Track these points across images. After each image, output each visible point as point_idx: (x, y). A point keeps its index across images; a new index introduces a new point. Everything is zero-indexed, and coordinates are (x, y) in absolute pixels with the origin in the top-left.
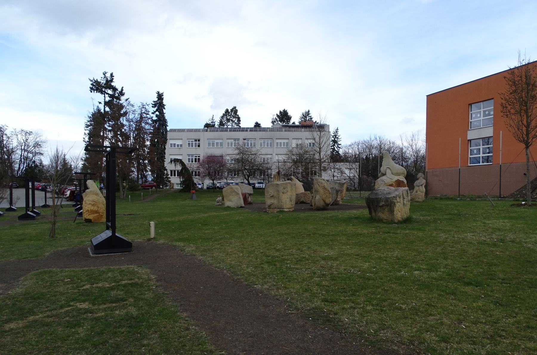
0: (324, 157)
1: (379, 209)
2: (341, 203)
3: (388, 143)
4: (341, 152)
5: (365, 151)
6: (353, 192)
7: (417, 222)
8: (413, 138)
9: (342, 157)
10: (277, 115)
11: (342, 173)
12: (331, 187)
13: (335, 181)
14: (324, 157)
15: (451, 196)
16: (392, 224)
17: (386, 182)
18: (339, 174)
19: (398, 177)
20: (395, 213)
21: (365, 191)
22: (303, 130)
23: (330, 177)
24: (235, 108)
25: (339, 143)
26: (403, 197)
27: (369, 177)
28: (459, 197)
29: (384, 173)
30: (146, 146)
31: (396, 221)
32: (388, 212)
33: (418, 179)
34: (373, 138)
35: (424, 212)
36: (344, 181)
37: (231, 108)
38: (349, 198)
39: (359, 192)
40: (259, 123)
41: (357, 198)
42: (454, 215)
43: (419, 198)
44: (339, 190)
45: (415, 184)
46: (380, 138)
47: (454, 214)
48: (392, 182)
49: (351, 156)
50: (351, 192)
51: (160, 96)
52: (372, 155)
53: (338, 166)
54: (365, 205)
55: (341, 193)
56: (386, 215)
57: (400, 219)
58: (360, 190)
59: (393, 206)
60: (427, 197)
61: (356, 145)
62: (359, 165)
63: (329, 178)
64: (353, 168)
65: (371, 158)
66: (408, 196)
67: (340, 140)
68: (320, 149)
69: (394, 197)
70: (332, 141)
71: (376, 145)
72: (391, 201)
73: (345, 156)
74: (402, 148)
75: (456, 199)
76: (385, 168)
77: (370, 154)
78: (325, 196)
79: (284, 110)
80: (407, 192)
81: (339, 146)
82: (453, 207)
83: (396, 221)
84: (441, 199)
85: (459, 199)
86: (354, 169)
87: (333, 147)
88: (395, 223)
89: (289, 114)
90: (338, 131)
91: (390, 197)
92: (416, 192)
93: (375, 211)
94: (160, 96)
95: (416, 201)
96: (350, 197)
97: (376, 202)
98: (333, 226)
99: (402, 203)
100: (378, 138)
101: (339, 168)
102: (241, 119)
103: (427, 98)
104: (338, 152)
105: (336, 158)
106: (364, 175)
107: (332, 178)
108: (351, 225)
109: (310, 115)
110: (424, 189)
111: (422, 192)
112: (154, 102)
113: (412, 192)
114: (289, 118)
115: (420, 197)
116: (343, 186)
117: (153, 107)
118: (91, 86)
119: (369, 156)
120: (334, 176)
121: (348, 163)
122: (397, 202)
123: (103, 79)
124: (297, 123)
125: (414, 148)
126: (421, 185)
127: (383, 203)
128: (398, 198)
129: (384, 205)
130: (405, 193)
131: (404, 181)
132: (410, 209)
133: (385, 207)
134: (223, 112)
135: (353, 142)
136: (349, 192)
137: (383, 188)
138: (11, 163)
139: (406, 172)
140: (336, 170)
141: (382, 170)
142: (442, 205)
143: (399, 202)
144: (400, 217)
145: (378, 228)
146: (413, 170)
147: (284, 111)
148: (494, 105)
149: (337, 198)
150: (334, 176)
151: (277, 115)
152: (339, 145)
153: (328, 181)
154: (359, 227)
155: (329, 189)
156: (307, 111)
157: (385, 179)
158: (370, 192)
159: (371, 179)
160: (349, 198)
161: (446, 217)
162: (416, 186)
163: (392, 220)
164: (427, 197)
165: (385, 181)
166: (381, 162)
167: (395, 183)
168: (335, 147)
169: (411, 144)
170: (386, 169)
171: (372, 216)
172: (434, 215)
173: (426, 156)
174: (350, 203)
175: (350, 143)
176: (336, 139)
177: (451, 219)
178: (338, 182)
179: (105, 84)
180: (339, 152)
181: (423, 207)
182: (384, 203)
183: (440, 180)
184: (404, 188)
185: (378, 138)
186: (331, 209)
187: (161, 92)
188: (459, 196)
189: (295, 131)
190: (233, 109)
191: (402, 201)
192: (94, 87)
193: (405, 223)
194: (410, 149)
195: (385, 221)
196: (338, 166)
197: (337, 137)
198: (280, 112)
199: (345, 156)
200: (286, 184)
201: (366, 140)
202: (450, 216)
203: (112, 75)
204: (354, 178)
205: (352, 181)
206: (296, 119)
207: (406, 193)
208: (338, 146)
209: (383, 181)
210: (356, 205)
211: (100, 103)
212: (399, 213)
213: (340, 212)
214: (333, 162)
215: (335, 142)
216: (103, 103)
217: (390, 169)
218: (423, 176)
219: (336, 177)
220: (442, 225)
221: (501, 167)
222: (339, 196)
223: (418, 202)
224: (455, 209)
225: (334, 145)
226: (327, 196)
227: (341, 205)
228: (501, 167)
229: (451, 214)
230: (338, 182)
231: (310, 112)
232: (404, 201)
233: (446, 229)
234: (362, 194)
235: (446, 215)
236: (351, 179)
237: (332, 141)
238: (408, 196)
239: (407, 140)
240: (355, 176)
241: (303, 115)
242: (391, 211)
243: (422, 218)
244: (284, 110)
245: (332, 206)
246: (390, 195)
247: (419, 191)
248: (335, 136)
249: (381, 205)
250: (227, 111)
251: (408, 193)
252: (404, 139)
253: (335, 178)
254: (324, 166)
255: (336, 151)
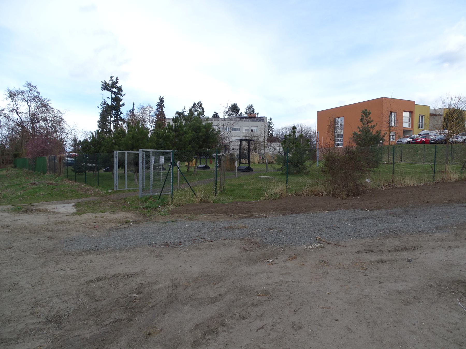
4: (274, 134)
9: (274, 137)
10: (230, 107)
22: (250, 120)
24: (200, 102)
25: (273, 128)
30: (293, 154)
37: (198, 102)
40: (217, 112)
46: (301, 125)
49: (281, 137)
51: (162, 100)
67: (273, 125)
68: (264, 138)
79: (235, 103)
81: (273, 130)
89: (238, 107)
90: (271, 119)
94: (162, 100)
100: (299, 125)
102: (205, 110)
103: (317, 113)
105: (271, 139)
109: (253, 108)
112: (158, 103)
114: (238, 110)
117: (157, 106)
118: (102, 86)
120: (270, 151)
123: (110, 81)
124: (244, 115)
134: (192, 105)
138: (88, 141)
147: (235, 104)
148: (344, 119)
151: (230, 107)
152: (273, 129)
156: (251, 105)
168: (269, 130)
176: (270, 125)
179: (112, 85)
185: (299, 125)
187: (162, 97)
189: (244, 121)
190: (199, 103)
192: (104, 87)
197: (271, 123)
198: (232, 105)
200: (256, 154)
203: (117, 78)
206: (243, 110)
208: (272, 130)
211: (108, 98)
215: (270, 127)
216: (111, 98)
231: (253, 106)
241: (248, 107)
244: (235, 103)
248: (270, 123)
250: (195, 104)
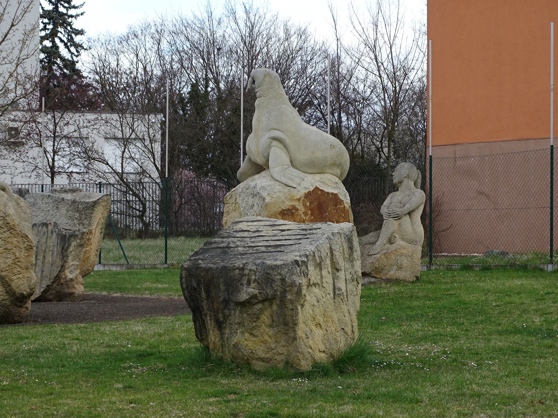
0: (12, 86)
1: (236, 316)
2: (79, 289)
3: (282, 35)
5: (186, 64)
6: (136, 242)
7: (389, 366)
8: (381, 18)
11: (89, 158)
12: (38, 220)
13: (57, 195)
14: (12, 86)
15: (525, 257)
16: (290, 377)
17: (268, 200)
18: (78, 161)
19: (318, 177)
20: (300, 333)
21: (189, 235)
23: (38, 176)
25: (77, 24)
26: (332, 260)
27: (206, 175)
28: (551, 262)
29: (260, 160)
31: (305, 365)
32: (270, 326)
33: (395, 188)
34: (219, 12)
35: (416, 326)
36: (96, 195)
38: (118, 269)
39: (160, 242)
41: (154, 267)
42: (530, 333)
43: (400, 268)
44: (73, 236)
45: (384, 210)
46: (247, 12)
47: (530, 332)
48: (292, 199)
49: (128, 85)
50: (126, 243)
52: (217, 82)
53: (68, 130)
54: (178, 296)
55: (81, 246)
56: (265, 342)
57: (321, 357)
58: (166, 236)
59: (292, 302)
60: (430, 262)
61: (148, 38)
62: (163, 123)
63: (32, 181)
64: (137, 138)
65: (213, 96)
66: (351, 260)
67: (78, 11)
69: (296, 262)
70: (42, 16)
71: (231, 42)
72: (283, 280)
73: (102, 82)
74: (338, 57)
75: (542, 270)
76: (264, 139)
77: (207, 80)
78: (10, 261)
80: (349, 240)
81: (78, 39)
82: (527, 301)
83: (305, 365)
84: (486, 268)
85: (550, 268)
86: (143, 140)
87: (48, 43)
88: (300, 374)
91: (279, 263)
92: (391, 241)
93: (220, 325)
95: (389, 281)
96: (123, 261)
97: (222, 287)
98: (41, 396)
99: (330, 288)
100: (241, 14)
101: (76, 134)
104: (73, 63)
106: (185, 167)
107: (48, 180)
108: (120, 386)
110: (421, 229)
111: (410, 242)
113: (374, 243)
115: (405, 262)
116: (89, 217)
119: (207, 86)
120: (53, 174)
121: (115, 116)
122: (309, 285)
125: (384, 56)
126: (409, 214)
127: (252, 290)
128: (311, 268)
129: (254, 297)
130: (340, 247)
131: (342, 198)
132: (360, 314)
133: (260, 306)
135: (136, 22)
136: (115, 243)
137: (253, 227)
139: (346, 158)
140: (64, 143)
141: (252, 149)
142: (486, 292)
143: (315, 285)
144: (322, 348)
145: (233, 397)
146: (379, 150)
149: (63, 268)
150: (53, 174)
153: (22, 193)
154: (152, 393)
155: (26, 228)
157: (263, 188)
158: (197, 244)
159: (214, 187)
160: (118, 269)
161: (498, 342)
162: (389, 215)
163: (287, 363)
164: (430, 262)
165: (264, 194)
166: (250, 111)
167: (304, 205)
168: (57, 41)
169: (372, 42)
170: (269, 146)
171: (207, 347)
172: (455, 338)
173: (428, 86)
174: (120, 290)
175: (123, 31)
176: (61, 9)
177: (517, 351)
178: (69, 197)
180: (78, 66)
181: (415, 303)
182: (257, 292)
183: (482, 193)
184: (336, 227)
185: (241, 14)
186: (35, 320)
188: (551, 256)
191: (328, 279)
193: (341, 372)
194: (367, 61)
195: (258, 366)
196: (71, 128)
199: (103, 86)
201: (190, 17)
202: (517, 338)
204: (140, 183)
205: (134, 194)
207: (346, 246)
208: (71, 40)
209: (254, 195)
210: (143, 299)
212: (318, 332)
213: (75, 329)
214: (51, 108)
217: (286, 147)
218: (416, 173)
219: (65, 176)
220: (485, 377)
221: (552, 153)
222: (71, 262)
223: (397, 281)
224: (536, 311)
225: (53, 34)
226: (16, 261)
227: (84, 298)
228: (552, 153)
229: (517, 331)
230: (69, 197)
232: (335, 278)
233: (496, 391)
234: (173, 249)
235: (500, 333)
236: (127, 185)
237: (46, 14)
238: (351, 260)
239: (356, 23)
240: (143, 172)
242: (286, 324)
243: (407, 348)
245: (38, 305)
246: (280, 256)
247: (403, 239)
249: (243, 296)
251: (351, 248)
252: (343, 22)
253: (61, 180)
254: (11, 124)
255: (63, 59)
